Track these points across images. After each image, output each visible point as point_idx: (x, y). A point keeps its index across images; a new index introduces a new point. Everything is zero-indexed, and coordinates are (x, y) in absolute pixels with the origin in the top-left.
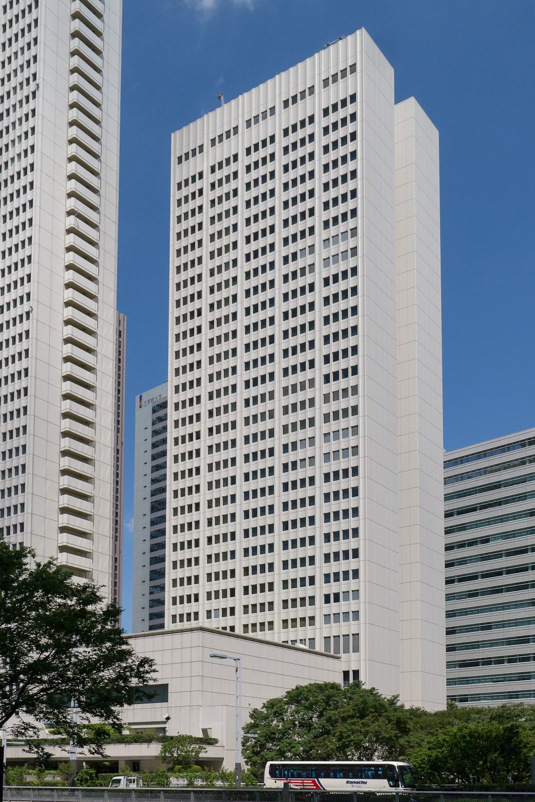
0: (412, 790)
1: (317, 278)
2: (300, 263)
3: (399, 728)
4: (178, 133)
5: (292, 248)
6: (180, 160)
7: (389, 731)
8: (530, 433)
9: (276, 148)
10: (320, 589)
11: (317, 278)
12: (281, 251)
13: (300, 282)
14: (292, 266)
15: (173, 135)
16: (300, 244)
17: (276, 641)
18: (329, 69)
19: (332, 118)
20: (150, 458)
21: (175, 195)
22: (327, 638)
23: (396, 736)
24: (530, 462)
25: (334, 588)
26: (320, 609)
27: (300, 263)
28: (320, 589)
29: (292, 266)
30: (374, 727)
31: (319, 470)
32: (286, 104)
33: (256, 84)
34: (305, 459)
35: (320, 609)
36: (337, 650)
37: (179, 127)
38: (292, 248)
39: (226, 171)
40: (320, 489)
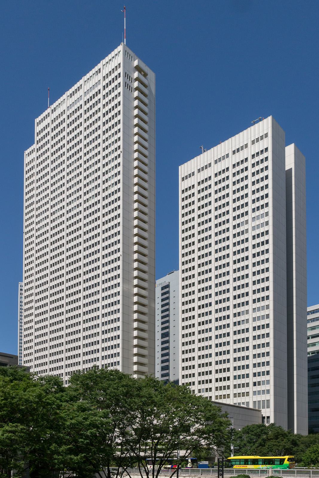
0: (107, 366)
1: (249, 235)
2: (242, 228)
3: (293, 444)
4: (182, 166)
5: (238, 221)
6: (266, 135)
7: (288, 445)
8: (316, 307)
9: (212, 182)
10: (251, 380)
11: (249, 235)
12: (232, 223)
13: (242, 237)
14: (238, 230)
15: (180, 167)
16: (242, 220)
17: (232, 404)
18: (264, 131)
19: (257, 159)
20: (160, 318)
21: (181, 196)
22: (255, 402)
23: (292, 448)
24: (317, 320)
25: (257, 379)
26: (251, 389)
27: (242, 228)
28: (251, 380)
29: (238, 230)
30: (282, 443)
31: (250, 325)
32: (234, 152)
33: (238, 133)
34: (244, 320)
35: (251, 389)
36: (259, 407)
37: (183, 163)
38: (238, 221)
39: (223, 176)
40: (251, 334)
